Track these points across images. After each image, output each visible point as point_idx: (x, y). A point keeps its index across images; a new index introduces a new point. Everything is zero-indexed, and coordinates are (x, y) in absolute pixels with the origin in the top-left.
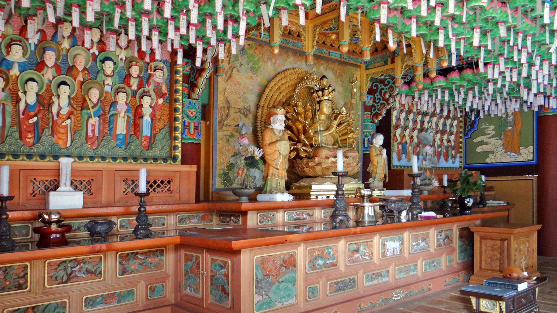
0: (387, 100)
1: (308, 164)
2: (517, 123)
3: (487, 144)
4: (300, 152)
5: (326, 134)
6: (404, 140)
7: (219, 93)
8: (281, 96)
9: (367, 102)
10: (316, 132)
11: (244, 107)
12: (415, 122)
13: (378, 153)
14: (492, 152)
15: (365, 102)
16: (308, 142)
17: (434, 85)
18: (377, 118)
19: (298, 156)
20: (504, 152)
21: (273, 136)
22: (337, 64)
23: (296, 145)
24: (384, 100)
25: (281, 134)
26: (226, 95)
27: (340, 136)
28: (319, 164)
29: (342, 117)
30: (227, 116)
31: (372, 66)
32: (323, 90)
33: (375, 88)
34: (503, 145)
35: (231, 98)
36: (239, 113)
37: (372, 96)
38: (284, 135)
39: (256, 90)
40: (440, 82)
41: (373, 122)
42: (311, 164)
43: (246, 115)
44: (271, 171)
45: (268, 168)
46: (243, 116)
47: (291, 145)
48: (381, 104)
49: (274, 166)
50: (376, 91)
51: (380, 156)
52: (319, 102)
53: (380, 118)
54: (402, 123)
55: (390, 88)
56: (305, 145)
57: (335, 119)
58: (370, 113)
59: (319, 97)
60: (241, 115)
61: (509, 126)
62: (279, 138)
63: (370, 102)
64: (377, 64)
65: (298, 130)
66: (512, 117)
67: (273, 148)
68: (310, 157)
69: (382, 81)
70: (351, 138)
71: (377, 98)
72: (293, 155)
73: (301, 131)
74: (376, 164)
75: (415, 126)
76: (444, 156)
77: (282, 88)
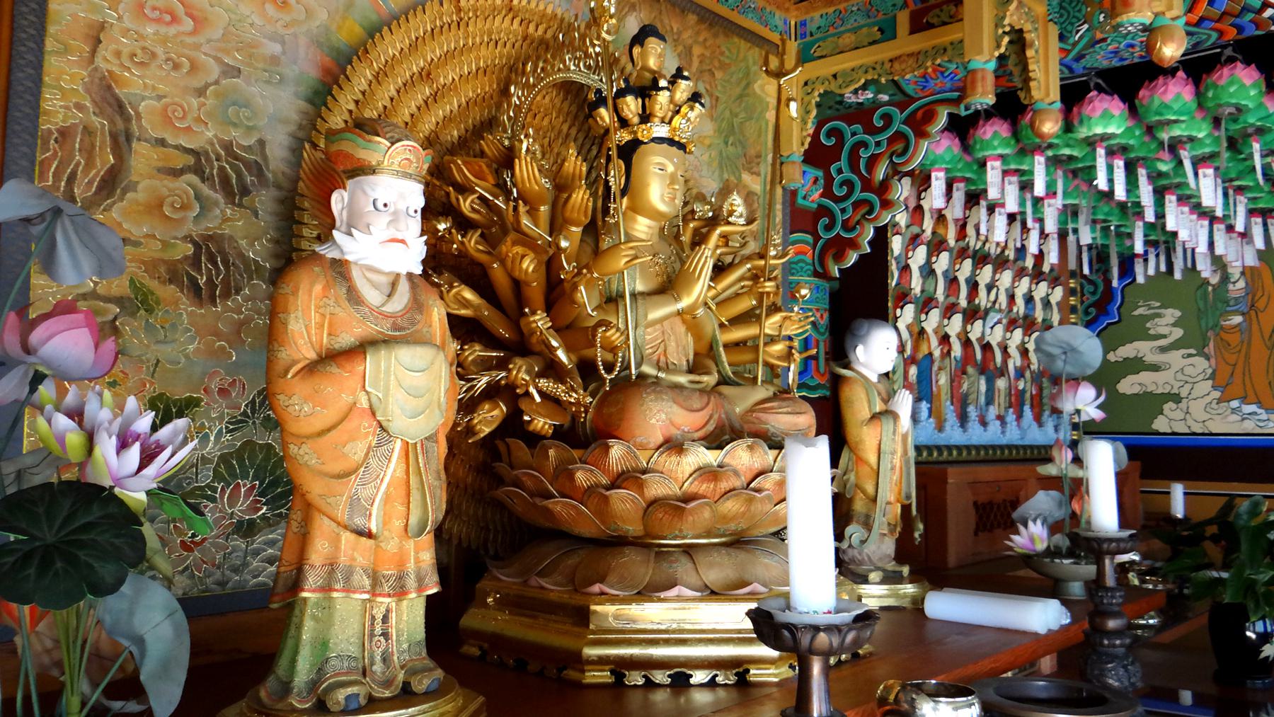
0: (884, 187)
1: (571, 476)
2: (1261, 304)
3: (1155, 368)
4: (523, 405)
5: (659, 312)
6: (924, 350)
7: (50, 44)
8: (440, 113)
9: (801, 193)
10: (612, 300)
11: (228, 146)
12: (952, 282)
13: (879, 407)
14: (1176, 398)
15: (794, 193)
16: (568, 350)
17: (1083, 132)
18: (839, 257)
19: (513, 425)
20: (1219, 401)
21: (344, 312)
22: (692, 18)
23: (502, 364)
24: (867, 185)
25: (400, 302)
26: (105, 60)
27: (722, 325)
28: (630, 478)
29: (725, 237)
30: (112, 183)
31: (827, 46)
32: (646, 91)
33: (832, 141)
34: (1213, 377)
35: (137, 86)
36: (194, 179)
37: (820, 174)
38: (417, 305)
39: (305, 66)
40: (1106, 116)
41: (822, 275)
42: (581, 477)
43: (235, 192)
44: (319, 552)
45: (306, 522)
46: (219, 197)
47: (462, 371)
48: (856, 205)
49: (342, 513)
50: (834, 154)
51: (887, 424)
52: (629, 151)
53: (852, 258)
54: (916, 284)
55: (891, 141)
56: (552, 369)
57: (699, 240)
58: (809, 238)
59: (624, 123)
60: (206, 190)
61: (1236, 312)
62: (385, 328)
63: (812, 197)
64: (848, 39)
65: (517, 285)
66: (1241, 284)
67: (339, 390)
68: (585, 436)
69: (861, 115)
70: (772, 340)
71: (838, 179)
72: (488, 418)
73: (536, 288)
74: (872, 459)
75: (952, 300)
76: (1032, 407)
77: (448, 76)
